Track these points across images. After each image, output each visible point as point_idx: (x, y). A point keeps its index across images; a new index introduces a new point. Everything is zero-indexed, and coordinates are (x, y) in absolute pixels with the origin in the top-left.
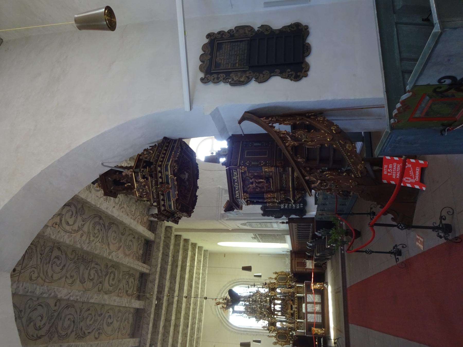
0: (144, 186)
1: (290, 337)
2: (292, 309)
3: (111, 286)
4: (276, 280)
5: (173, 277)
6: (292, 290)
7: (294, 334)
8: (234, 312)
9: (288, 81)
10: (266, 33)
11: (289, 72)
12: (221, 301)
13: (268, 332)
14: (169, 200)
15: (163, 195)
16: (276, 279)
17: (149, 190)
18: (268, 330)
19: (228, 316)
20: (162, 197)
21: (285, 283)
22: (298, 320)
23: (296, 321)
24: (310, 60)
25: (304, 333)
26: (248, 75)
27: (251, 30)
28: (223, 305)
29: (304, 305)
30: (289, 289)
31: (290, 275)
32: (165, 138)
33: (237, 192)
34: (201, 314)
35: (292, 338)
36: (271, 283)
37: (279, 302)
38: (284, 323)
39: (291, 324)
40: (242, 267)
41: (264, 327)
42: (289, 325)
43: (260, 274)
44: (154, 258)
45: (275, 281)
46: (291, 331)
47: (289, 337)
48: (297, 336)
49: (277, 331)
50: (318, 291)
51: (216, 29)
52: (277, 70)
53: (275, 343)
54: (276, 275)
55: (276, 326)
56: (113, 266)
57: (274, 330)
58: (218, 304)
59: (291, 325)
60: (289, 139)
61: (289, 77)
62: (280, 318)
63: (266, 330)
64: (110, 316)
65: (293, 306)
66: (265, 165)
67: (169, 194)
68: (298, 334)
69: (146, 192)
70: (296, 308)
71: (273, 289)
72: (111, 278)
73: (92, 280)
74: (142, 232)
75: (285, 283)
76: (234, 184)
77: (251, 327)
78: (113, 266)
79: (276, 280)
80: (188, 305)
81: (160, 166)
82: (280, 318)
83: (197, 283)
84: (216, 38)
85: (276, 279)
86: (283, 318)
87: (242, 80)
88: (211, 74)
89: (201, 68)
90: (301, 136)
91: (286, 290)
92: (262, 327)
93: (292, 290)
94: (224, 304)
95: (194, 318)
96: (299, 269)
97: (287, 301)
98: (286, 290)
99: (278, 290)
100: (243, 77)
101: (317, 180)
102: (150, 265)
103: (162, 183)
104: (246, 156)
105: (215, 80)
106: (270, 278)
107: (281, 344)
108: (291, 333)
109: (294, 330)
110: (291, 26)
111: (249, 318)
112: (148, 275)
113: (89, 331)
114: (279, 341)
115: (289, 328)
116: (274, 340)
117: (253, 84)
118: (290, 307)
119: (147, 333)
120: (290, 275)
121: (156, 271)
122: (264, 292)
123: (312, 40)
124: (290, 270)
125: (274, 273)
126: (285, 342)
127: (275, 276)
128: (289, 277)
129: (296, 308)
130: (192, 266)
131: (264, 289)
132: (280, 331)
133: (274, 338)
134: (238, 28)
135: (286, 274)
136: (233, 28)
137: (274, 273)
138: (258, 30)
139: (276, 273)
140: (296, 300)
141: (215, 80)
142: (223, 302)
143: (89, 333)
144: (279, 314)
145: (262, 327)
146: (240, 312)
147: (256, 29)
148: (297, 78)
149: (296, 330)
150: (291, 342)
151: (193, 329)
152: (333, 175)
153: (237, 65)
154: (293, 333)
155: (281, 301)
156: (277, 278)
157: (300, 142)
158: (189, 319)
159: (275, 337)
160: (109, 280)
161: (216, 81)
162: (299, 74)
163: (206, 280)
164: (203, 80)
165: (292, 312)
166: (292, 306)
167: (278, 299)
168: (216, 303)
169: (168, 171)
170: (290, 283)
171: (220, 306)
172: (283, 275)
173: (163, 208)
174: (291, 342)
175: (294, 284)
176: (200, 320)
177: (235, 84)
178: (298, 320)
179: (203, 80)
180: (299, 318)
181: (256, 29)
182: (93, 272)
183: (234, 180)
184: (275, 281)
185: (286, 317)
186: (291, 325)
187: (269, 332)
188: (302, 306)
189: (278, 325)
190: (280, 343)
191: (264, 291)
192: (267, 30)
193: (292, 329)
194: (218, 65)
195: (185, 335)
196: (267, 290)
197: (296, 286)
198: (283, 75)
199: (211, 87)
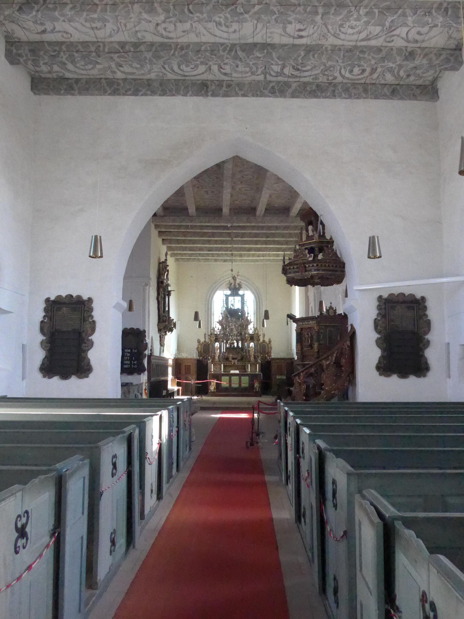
0: (303, 254)
1: (205, 357)
2: (233, 359)
3: (239, 189)
4: (262, 342)
5: (256, 235)
6: (252, 359)
7: (209, 362)
8: (227, 296)
9: (376, 362)
10: (421, 345)
11: (384, 362)
12: (238, 281)
13: (209, 334)
14: (294, 272)
15: (297, 268)
16: (264, 341)
17: (300, 258)
18: (211, 334)
19: (223, 289)
20: (295, 267)
21: (260, 351)
22: (222, 365)
23: (222, 364)
24: (394, 378)
25: (211, 371)
26: (382, 332)
27: (425, 333)
28: (233, 284)
29: (237, 372)
30: (253, 356)
31: (268, 358)
32: (344, 264)
33: (301, 323)
34: (223, 261)
35: (205, 359)
36: (259, 336)
37: (240, 345)
38: (219, 351)
39: (218, 358)
40: (268, 310)
41: (214, 329)
42: (218, 355)
43: (265, 326)
44: (272, 219)
45: (261, 340)
46: (211, 357)
47: (206, 356)
48: (207, 364)
49: (210, 343)
50: (251, 386)
51: (430, 304)
52: (386, 353)
53: (199, 341)
54: (268, 342)
55: (216, 342)
56: (258, 188)
57: (211, 340)
58: (234, 278)
59: (217, 358)
60: (328, 363)
61: (379, 362)
62: (224, 346)
63: (211, 332)
64: (213, 192)
65: (236, 360)
66: (319, 344)
67: (298, 272)
68: (209, 364)
69: (299, 255)
70: (234, 363)
71: (252, 338)
72: (246, 189)
73: (243, 177)
74: (295, 206)
75: (260, 351)
76: (307, 321)
77: (213, 314)
78: (258, 188)
79: (262, 342)
80: (229, 250)
81: (317, 265)
82: (224, 346)
83: (253, 255)
84: (420, 304)
85: (264, 341)
86: (223, 350)
87: (379, 328)
88: (385, 303)
89: (391, 295)
90: (329, 371)
91: (252, 353)
92: (213, 328)
93: (252, 359)
94: (235, 285)
95: (218, 255)
96: (274, 368)
97: (241, 354)
98: (252, 353)
99: (252, 344)
100: (381, 329)
101: (301, 380)
102: (264, 215)
103: (305, 267)
104: (329, 330)
105: (379, 307)
106: (264, 335)
107: (198, 348)
108: (209, 357)
109: (212, 362)
110: (426, 363)
111: (222, 314)
112: (255, 215)
113: (200, 181)
114: (201, 346)
115: (214, 356)
116: (202, 340)
117: (376, 336)
118: (235, 356)
119: (201, 222)
120: (268, 358)
121: (259, 222)
122: (249, 328)
123: (412, 379)
124: (273, 357)
125: (270, 339)
126: (201, 351)
127: (267, 340)
128: (266, 356)
129: (234, 363)
130: (270, 250)
131: (253, 329)
132: (211, 346)
133: (204, 340)
134: (428, 323)
135: (269, 353)
136: (429, 318)
137: (270, 339)
138: (424, 338)
139: (270, 341)
140: (240, 364)
141: (379, 307)
142: (237, 285)
143: (199, 181)
144: (227, 345)
145: (213, 328)
146: (227, 303)
147: (427, 337)
148: (378, 368)
149: (212, 363)
150: (201, 358)
151: (208, 255)
152: (303, 391)
153: (392, 323)
154: (209, 360)
155: (240, 346)
156: (264, 342)
157: (325, 370)
158: (216, 251)
159: (205, 341)
160: (245, 187)
161: (379, 307)
162: (382, 370)
163: (258, 263)
164: (380, 298)
165: (230, 359)
166: (235, 359)
167: (243, 344)
168: (235, 277)
169: (315, 271)
170: (260, 357)
171: (232, 281)
172: (268, 348)
173: (288, 268)
174: (201, 358)
175: (259, 361)
176: (216, 260)
177: (376, 321)
178: (222, 365)
179: (380, 298)
180: (224, 366)
181: (427, 337)
182: (250, 177)
183: (309, 321)
184: (261, 340)
185: (225, 353)
186: (217, 358)
187: (209, 335)
188: (237, 370)
189: (217, 344)
190: (200, 346)
191: (251, 329)
192: (424, 345)
193: (213, 358)
194: (393, 308)
195: (201, 249)
196: (251, 332)
197: (257, 364)
198: (382, 358)
199: (375, 303)
